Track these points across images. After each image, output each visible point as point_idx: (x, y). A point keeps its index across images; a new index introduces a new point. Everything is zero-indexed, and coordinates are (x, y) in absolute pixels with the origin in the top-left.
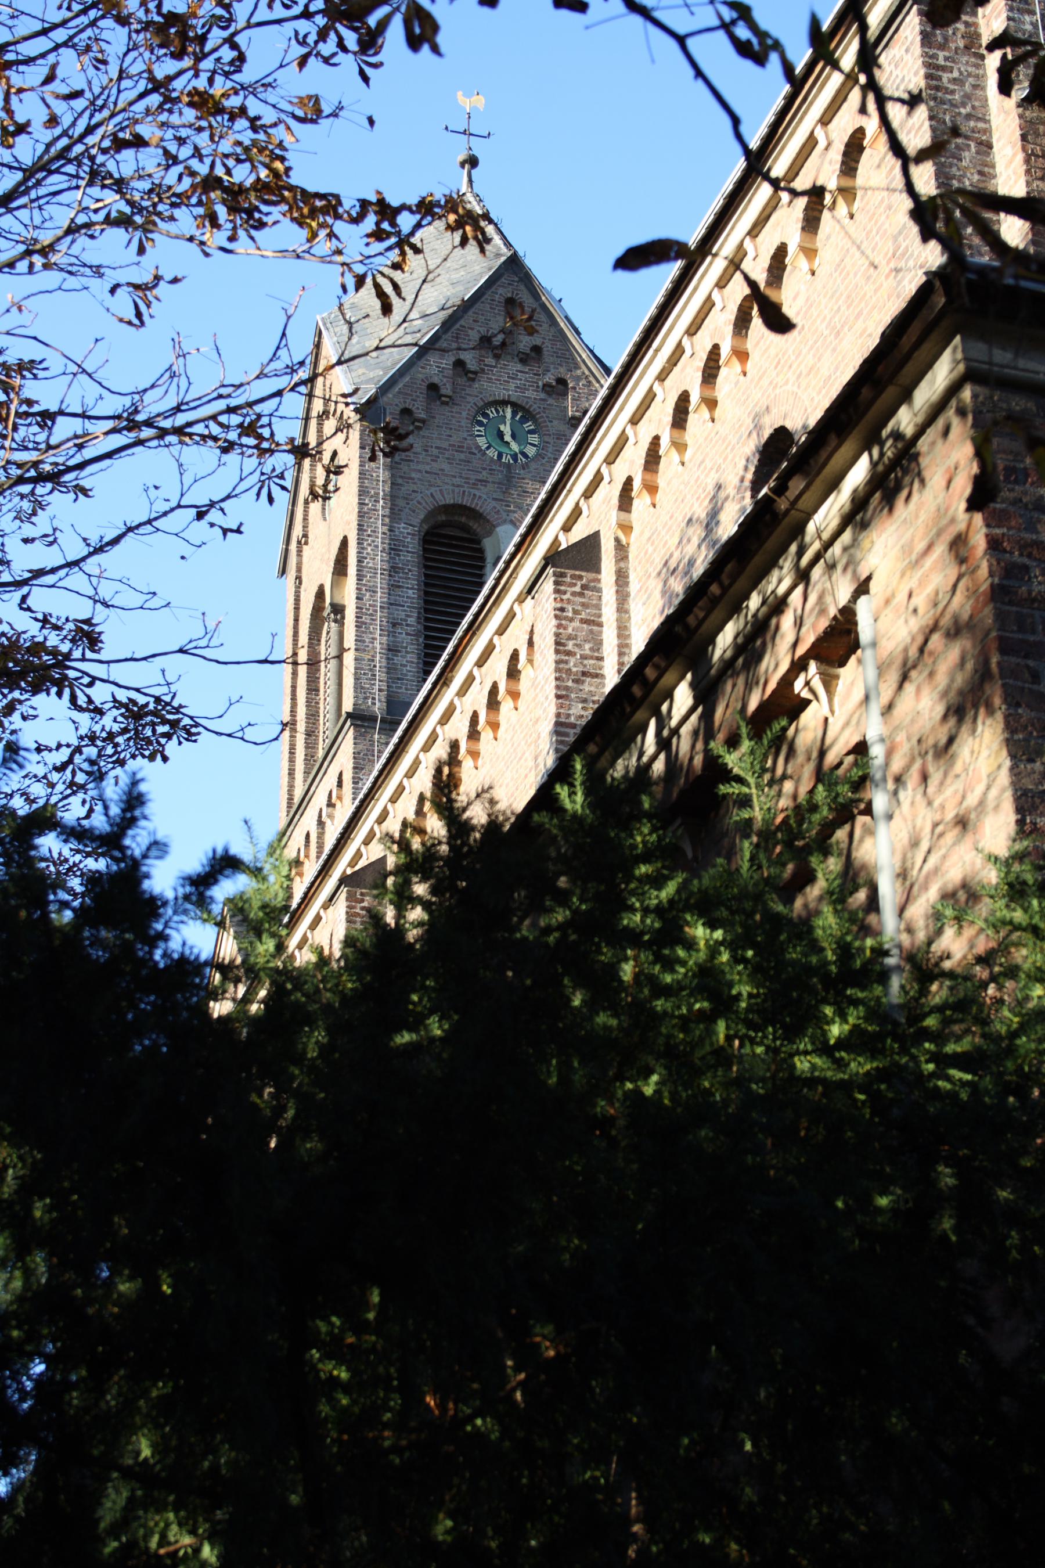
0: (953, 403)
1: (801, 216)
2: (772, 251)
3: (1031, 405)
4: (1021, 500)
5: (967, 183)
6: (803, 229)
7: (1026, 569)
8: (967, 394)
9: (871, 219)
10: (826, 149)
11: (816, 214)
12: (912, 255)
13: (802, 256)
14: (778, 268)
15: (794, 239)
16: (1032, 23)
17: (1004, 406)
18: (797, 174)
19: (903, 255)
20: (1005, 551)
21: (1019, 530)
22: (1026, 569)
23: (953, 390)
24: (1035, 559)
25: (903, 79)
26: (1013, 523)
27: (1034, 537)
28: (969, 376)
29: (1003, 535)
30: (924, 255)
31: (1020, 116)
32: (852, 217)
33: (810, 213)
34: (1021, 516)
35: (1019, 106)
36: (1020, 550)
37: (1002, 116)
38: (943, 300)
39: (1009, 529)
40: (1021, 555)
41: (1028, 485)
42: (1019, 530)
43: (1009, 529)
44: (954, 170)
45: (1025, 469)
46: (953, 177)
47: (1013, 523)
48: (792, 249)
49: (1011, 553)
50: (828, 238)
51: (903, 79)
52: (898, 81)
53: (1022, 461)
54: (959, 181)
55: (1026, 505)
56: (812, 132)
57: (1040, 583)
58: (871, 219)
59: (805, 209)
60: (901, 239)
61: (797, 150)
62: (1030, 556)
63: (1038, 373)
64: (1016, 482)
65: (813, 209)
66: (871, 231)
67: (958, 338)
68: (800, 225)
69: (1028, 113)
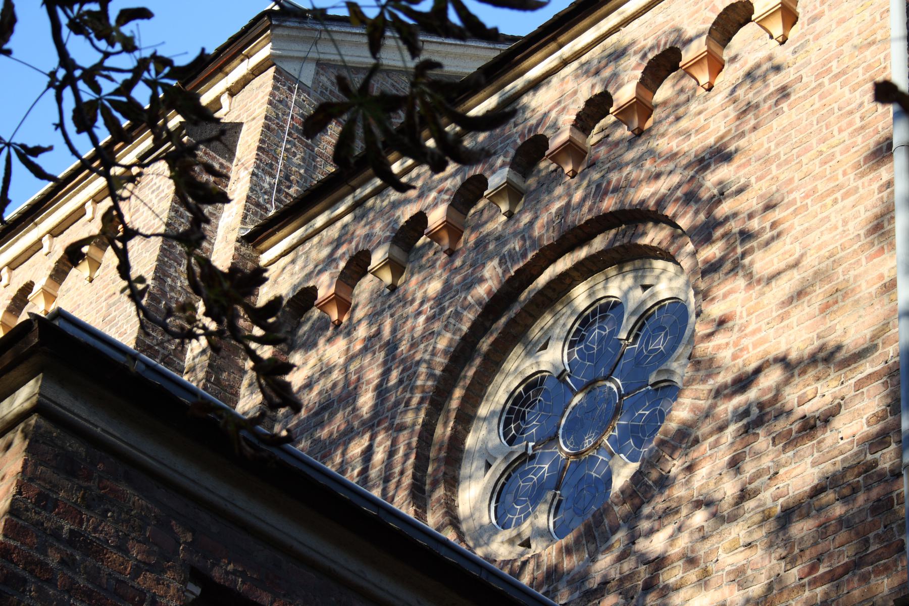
0: (21, 426)
1: (53, 266)
2: (21, 285)
3: (82, 450)
4: (42, 524)
5: (179, 284)
6: (51, 276)
7: (25, 581)
8: (33, 420)
9: (105, 287)
10: (90, 221)
11: (65, 268)
12: (117, 324)
13: (42, 297)
14: (21, 300)
15: (41, 281)
16: (270, 184)
17: (59, 443)
18: (62, 232)
19: (111, 321)
20: (12, 561)
21: (31, 548)
22: (25, 581)
23: (22, 416)
24: (36, 576)
25: (159, 187)
26: (28, 541)
27: (42, 558)
28: (38, 408)
29: (16, 547)
30: (125, 327)
31: (236, 249)
32: (91, 281)
33: (61, 266)
34: (37, 537)
35: (238, 241)
36: (25, 564)
37: (224, 243)
38: (36, 340)
39: (23, 544)
40: (24, 569)
41: (53, 514)
42: (31, 548)
43: (23, 544)
44: (172, 270)
45: (57, 500)
46: (169, 276)
47: (28, 541)
48: (36, 289)
49: (17, 564)
50: (68, 291)
51: (159, 187)
52: (155, 187)
53: (57, 493)
54: (173, 280)
55: (46, 529)
56: (84, 204)
57: (31, 598)
58: (105, 287)
59: (57, 262)
60: (113, 308)
61: (68, 213)
62: (31, 572)
63: (97, 427)
64: (44, 508)
65: (64, 264)
66: (101, 297)
67: (41, 375)
68: (49, 273)
69: (243, 249)
